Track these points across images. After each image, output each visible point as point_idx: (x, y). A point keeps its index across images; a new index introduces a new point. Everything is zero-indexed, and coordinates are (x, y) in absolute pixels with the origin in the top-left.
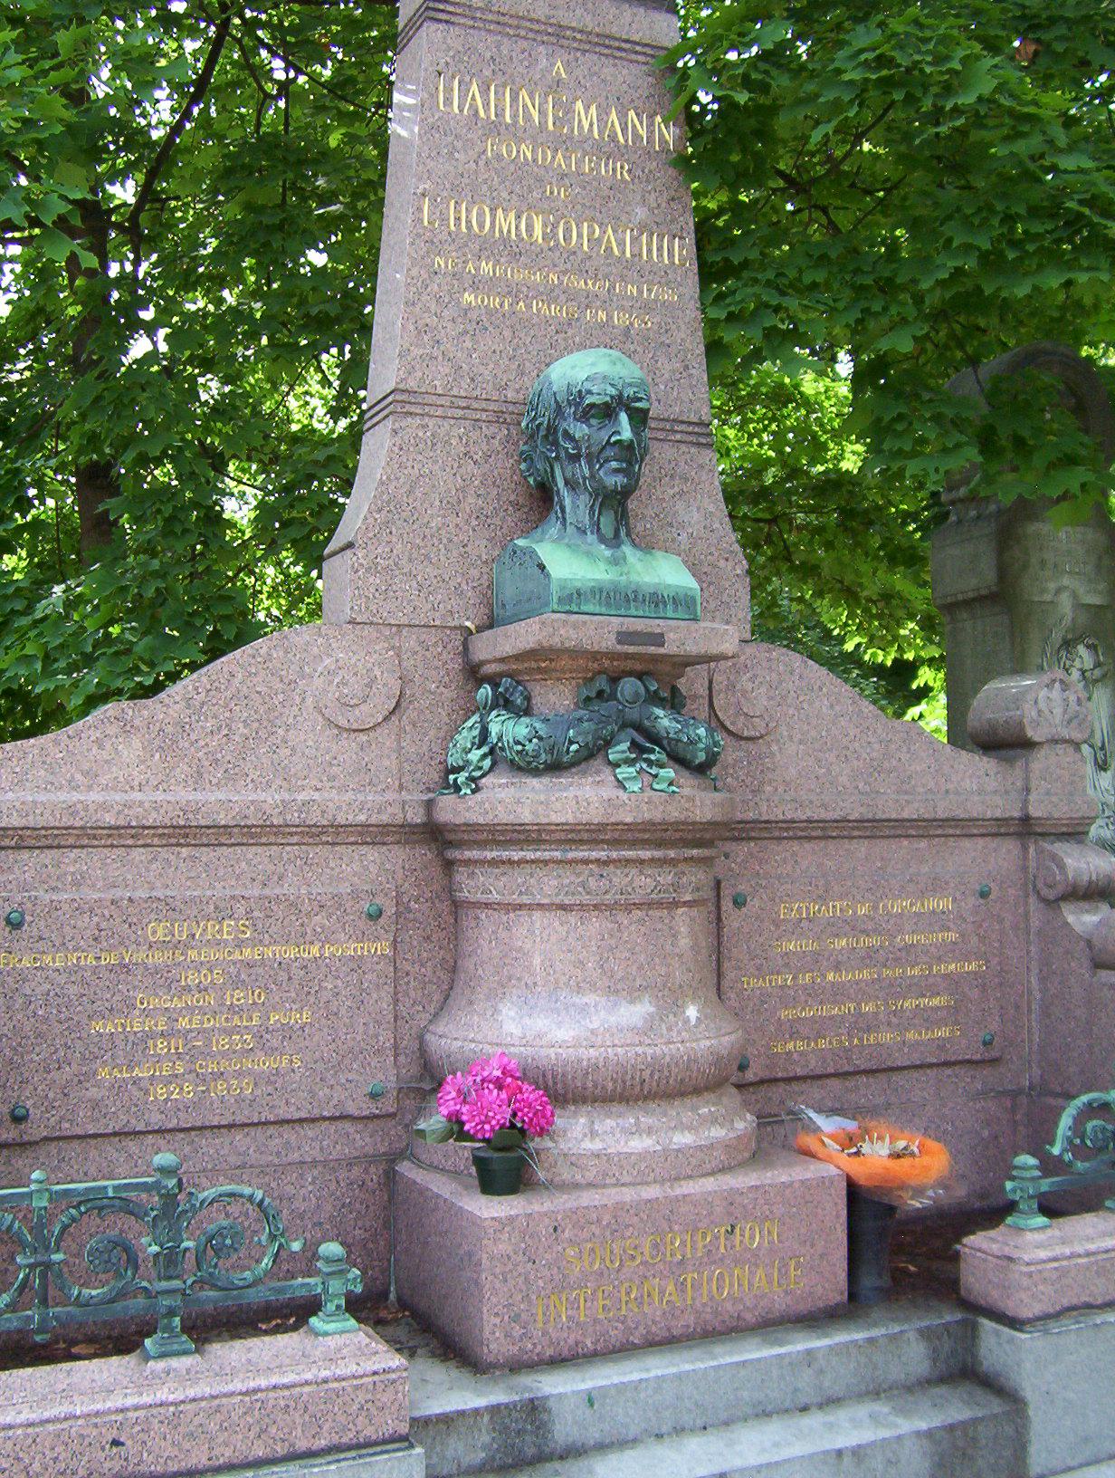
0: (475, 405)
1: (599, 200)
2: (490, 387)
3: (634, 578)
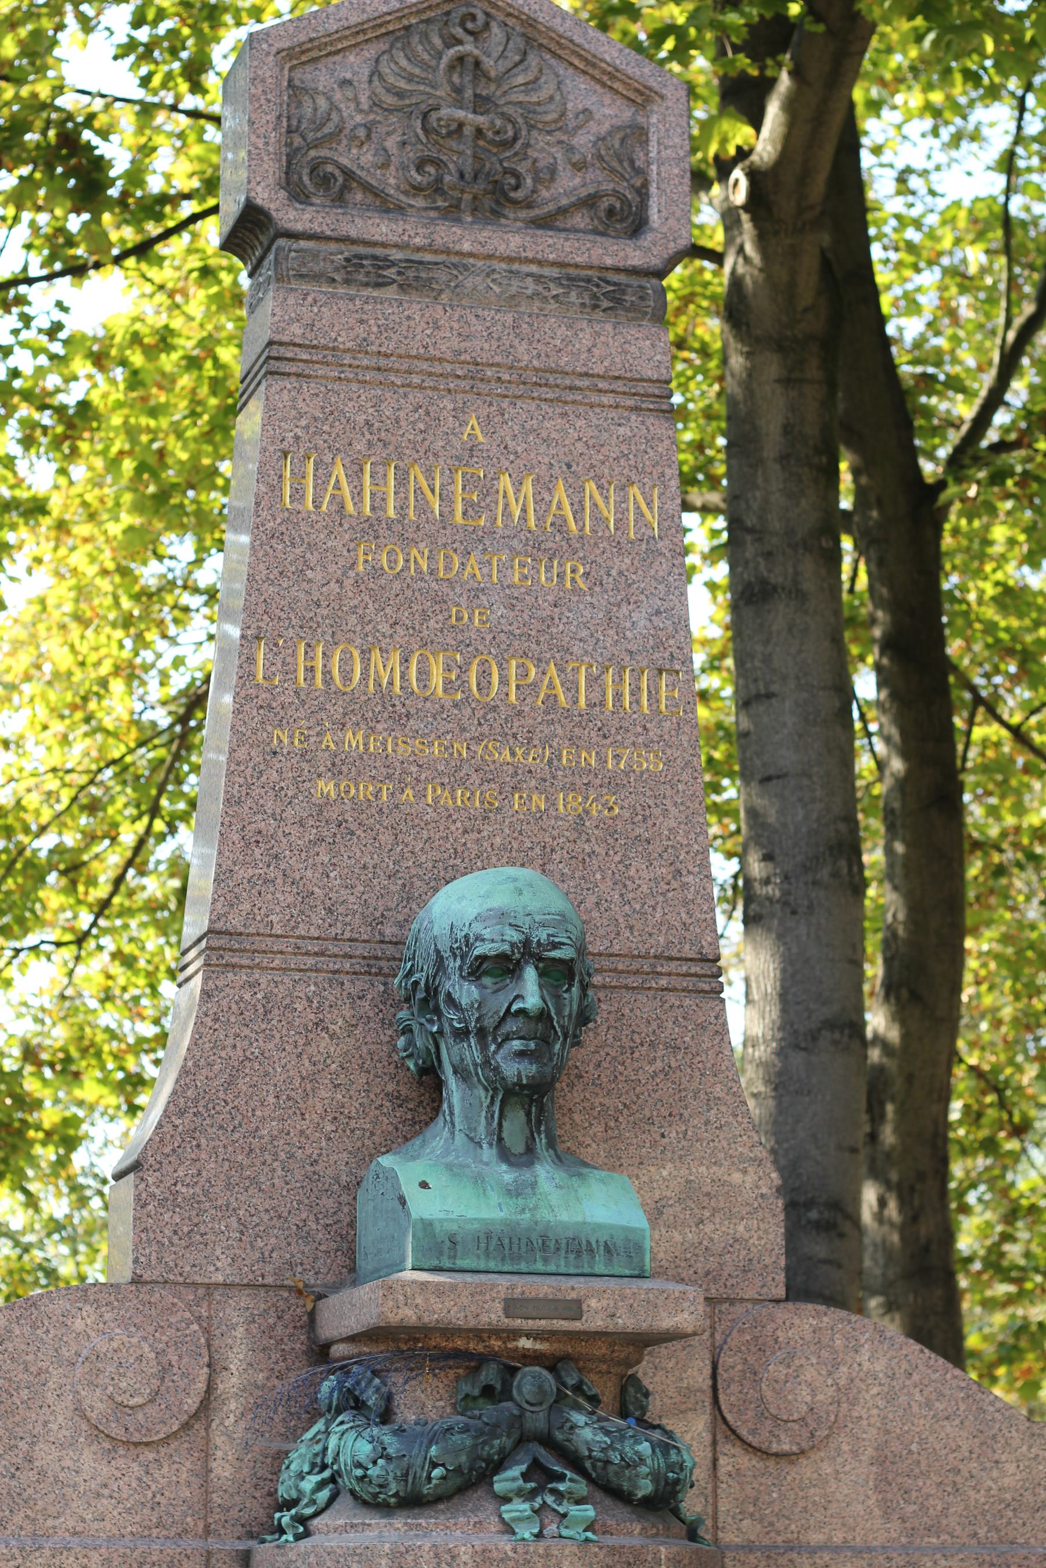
0: (333, 949)
1: (536, 625)
2: (357, 921)
3: (544, 1215)
